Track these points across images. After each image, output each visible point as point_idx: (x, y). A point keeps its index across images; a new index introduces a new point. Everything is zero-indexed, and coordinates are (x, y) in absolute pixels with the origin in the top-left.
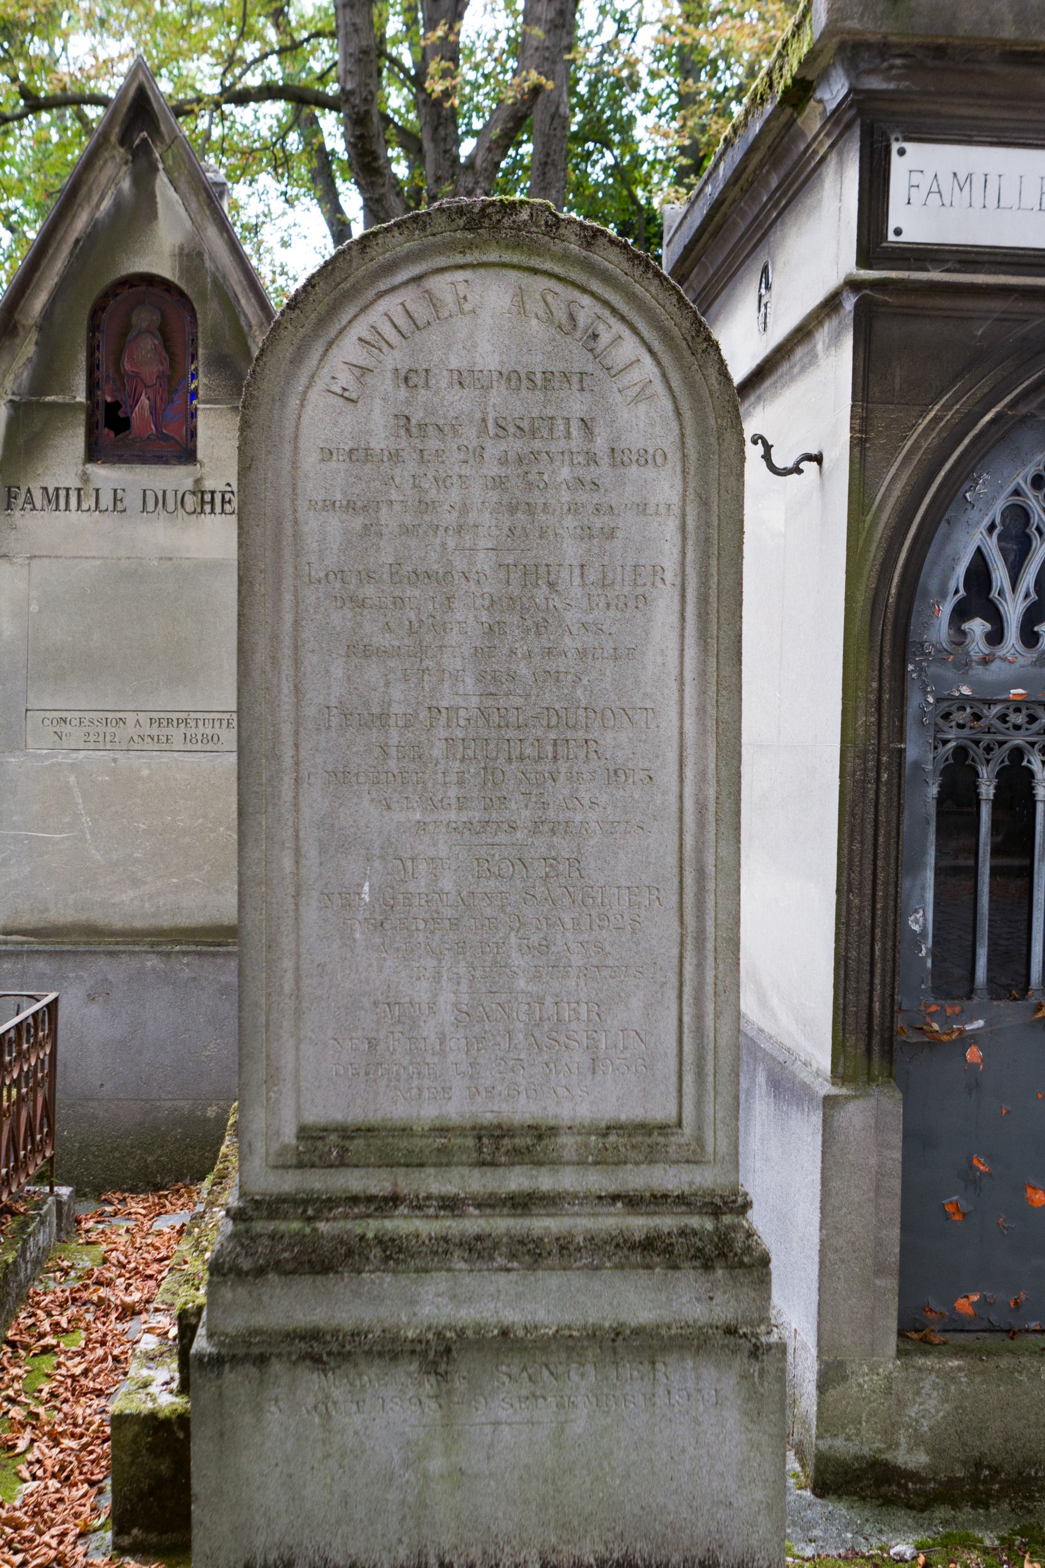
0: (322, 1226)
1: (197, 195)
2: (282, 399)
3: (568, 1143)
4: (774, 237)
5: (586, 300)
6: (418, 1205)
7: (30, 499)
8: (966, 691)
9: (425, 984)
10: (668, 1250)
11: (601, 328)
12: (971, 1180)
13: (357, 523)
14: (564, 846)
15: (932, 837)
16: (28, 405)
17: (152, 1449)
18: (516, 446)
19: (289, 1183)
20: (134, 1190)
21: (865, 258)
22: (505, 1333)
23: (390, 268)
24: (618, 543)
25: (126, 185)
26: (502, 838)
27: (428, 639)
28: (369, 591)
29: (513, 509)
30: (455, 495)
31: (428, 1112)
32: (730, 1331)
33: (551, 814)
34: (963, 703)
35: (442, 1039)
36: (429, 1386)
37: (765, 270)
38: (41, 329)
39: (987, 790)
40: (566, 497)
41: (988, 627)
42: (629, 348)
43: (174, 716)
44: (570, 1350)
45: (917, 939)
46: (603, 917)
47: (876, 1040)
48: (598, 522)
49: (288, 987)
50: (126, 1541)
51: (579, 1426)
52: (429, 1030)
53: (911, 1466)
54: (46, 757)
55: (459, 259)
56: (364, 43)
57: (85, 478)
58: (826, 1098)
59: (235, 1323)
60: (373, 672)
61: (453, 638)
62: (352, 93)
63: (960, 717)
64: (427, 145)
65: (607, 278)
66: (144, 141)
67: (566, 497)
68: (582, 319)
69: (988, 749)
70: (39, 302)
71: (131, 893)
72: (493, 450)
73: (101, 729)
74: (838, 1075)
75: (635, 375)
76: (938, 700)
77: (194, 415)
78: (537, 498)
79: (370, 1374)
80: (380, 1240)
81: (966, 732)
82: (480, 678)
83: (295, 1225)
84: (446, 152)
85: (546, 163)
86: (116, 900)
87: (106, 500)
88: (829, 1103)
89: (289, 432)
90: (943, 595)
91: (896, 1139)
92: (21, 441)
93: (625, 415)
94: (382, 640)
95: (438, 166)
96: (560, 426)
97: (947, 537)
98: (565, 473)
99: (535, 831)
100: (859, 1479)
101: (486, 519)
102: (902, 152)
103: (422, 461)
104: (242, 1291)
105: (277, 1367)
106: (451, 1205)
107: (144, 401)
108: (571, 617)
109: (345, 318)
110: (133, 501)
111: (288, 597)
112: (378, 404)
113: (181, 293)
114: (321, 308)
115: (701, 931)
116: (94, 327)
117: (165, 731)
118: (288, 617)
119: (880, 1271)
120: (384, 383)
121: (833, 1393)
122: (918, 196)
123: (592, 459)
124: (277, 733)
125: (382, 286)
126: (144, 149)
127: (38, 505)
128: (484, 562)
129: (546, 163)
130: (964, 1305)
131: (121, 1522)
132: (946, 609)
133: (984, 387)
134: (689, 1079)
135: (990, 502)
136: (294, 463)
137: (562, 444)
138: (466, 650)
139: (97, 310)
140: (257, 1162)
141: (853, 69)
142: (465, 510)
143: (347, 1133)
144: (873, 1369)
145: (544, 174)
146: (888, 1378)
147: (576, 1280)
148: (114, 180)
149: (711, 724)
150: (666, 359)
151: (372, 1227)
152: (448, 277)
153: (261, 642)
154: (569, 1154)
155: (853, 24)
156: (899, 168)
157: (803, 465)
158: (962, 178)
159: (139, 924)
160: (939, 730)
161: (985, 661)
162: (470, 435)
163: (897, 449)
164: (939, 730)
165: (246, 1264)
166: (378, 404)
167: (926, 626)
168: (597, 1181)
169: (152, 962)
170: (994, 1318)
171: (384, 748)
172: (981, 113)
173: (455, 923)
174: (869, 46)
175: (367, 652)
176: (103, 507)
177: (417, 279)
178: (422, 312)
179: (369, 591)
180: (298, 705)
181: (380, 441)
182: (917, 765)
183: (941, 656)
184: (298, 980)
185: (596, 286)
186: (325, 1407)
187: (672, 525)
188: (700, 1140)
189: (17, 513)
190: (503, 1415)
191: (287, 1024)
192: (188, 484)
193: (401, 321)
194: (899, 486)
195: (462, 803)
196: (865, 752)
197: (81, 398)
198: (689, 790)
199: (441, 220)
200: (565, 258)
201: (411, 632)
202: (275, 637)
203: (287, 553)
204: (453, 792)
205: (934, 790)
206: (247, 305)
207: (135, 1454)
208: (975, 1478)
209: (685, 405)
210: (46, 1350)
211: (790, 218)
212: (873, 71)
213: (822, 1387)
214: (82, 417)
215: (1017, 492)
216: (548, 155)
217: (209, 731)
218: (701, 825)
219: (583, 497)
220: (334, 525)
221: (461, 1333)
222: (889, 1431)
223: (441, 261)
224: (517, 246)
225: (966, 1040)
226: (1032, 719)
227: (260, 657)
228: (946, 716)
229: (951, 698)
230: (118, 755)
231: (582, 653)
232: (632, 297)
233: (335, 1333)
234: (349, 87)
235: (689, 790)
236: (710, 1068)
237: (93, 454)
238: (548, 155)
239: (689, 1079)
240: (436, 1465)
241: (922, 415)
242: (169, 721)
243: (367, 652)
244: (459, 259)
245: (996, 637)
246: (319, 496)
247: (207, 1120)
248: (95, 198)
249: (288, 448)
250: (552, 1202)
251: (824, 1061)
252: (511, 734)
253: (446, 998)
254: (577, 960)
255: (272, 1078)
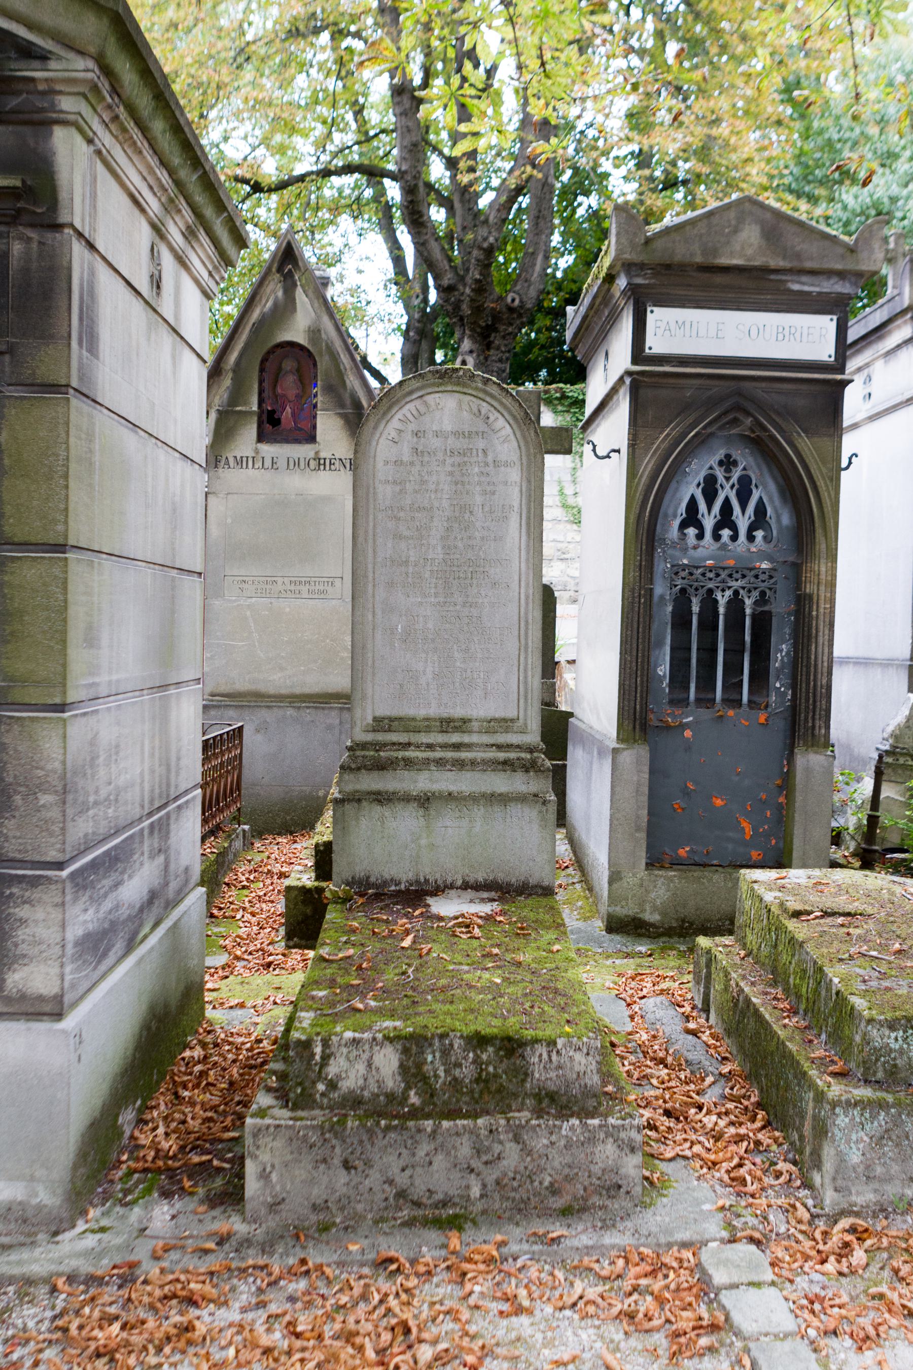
0: (382, 754)
1: (318, 298)
2: (370, 442)
3: (475, 725)
4: (609, 337)
5: (484, 404)
6: (418, 746)
7: (227, 462)
8: (685, 561)
9: (421, 664)
10: (512, 765)
11: (491, 415)
12: (686, 793)
13: (398, 488)
14: (475, 612)
15: (669, 631)
16: (227, 412)
17: (303, 902)
18: (458, 459)
19: (369, 737)
20: (279, 834)
21: (636, 359)
22: (450, 794)
23: (411, 393)
24: (496, 496)
25: (280, 294)
26: (451, 608)
27: (424, 532)
28: (402, 514)
29: (456, 483)
30: (434, 478)
31: (422, 713)
32: (536, 795)
33: (470, 599)
34: (684, 567)
35: (428, 684)
36: (421, 812)
37: (607, 354)
38: (234, 371)
39: (696, 609)
40: (476, 479)
41: (697, 531)
42: (501, 422)
43: (303, 579)
44: (474, 800)
45: (661, 679)
46: (490, 639)
47: (638, 722)
48: (488, 488)
49: (370, 663)
50: (291, 943)
51: (477, 829)
52: (423, 681)
53: (652, 920)
54: (235, 601)
55: (437, 389)
56: (414, 139)
57: (257, 451)
58: (614, 749)
59: (349, 788)
60: (403, 545)
61: (433, 532)
62: (405, 172)
63: (683, 574)
64: (457, 205)
65: (492, 396)
66: (290, 270)
67: (476, 479)
68: (483, 412)
69: (696, 589)
70: (233, 357)
71: (279, 675)
72: (449, 461)
73: (264, 586)
74: (619, 739)
75: (503, 433)
76: (672, 566)
77: (315, 417)
78: (466, 479)
79: (399, 806)
80: (403, 759)
81: (686, 581)
82: (443, 547)
83: (372, 753)
84: (470, 209)
85: (538, 217)
86: (271, 678)
87: (268, 463)
88: (615, 751)
89: (372, 454)
90: (675, 516)
91: (646, 769)
92: (223, 431)
93: (499, 448)
94: (406, 533)
95: (464, 219)
96: (474, 452)
97: (677, 489)
98: (476, 470)
99: (464, 606)
100: (627, 925)
101: (446, 487)
102: (652, 312)
103: (422, 465)
104: (352, 776)
105: (364, 803)
106: (430, 747)
107: (288, 409)
108: (478, 524)
109: (393, 411)
110: (282, 463)
111: (371, 517)
112: (406, 444)
113: (308, 351)
114: (385, 408)
115: (527, 644)
116: (262, 370)
117: (298, 588)
118: (371, 524)
119: (638, 829)
120: (408, 436)
121: (615, 886)
122: (660, 332)
123: (487, 464)
124: (366, 568)
125: (408, 399)
126: (290, 274)
127: (232, 465)
128: (445, 504)
129: (538, 217)
130: (682, 852)
131: (289, 936)
132: (676, 523)
133: (691, 419)
134: (522, 701)
135: (697, 474)
136: (374, 467)
137: (475, 459)
138: (439, 537)
139: (264, 360)
140: (357, 730)
141: (629, 274)
142: (438, 483)
143: (391, 720)
144: (634, 875)
145: (537, 224)
146: (641, 879)
147: (477, 775)
148: (274, 291)
149: (531, 566)
150: (515, 426)
151: (400, 754)
152: (433, 396)
153: (361, 533)
154: (475, 729)
155: (627, 256)
156: (651, 319)
157: (612, 454)
158: (680, 323)
159: (283, 691)
160: (673, 580)
161: (695, 548)
162: (440, 455)
163: (650, 448)
164: (673, 580)
165: (353, 766)
166: (406, 444)
167: (667, 531)
168: (486, 739)
169: (290, 712)
170: (696, 858)
171: (407, 574)
172: (690, 293)
173: (433, 640)
174: (635, 265)
175: (401, 537)
176: (266, 466)
177: (421, 396)
178: (422, 409)
179: (402, 514)
180: (375, 557)
181: (406, 458)
182: (662, 597)
183: (674, 545)
184: (374, 662)
185: (488, 399)
186: (382, 819)
187: (517, 490)
188: (526, 725)
189: (220, 470)
190: (448, 824)
191: (369, 678)
192: (312, 454)
193: (415, 413)
194: (650, 466)
195: (436, 595)
196: (634, 589)
197: (255, 408)
198: (523, 591)
199: (430, 375)
200: (476, 389)
201: (417, 530)
202: (366, 532)
203: (371, 500)
204: (433, 591)
205: (670, 609)
206: (344, 359)
207: (296, 904)
208: (682, 927)
209: (522, 444)
210: (244, 887)
211: (613, 331)
212: (637, 276)
213: (610, 883)
214: (255, 418)
215: (711, 468)
216: (540, 211)
217: (322, 588)
218: (527, 604)
219: (483, 479)
220: (389, 489)
221: (433, 794)
222: (642, 904)
223: (430, 390)
224: (458, 384)
225: (683, 727)
226: (718, 575)
227: (361, 539)
228: (676, 573)
229: (678, 565)
230: (273, 600)
231: (482, 538)
232: (501, 403)
233: (386, 792)
234: (404, 168)
235: (523, 591)
236: (529, 696)
237: (261, 438)
238: (540, 211)
239: (522, 701)
240: (423, 842)
241: (661, 433)
242: (300, 582)
243: (401, 537)
244: (437, 389)
245: (700, 536)
246: (383, 478)
247: (318, 797)
248: (264, 301)
249: (371, 460)
250: (469, 746)
251: (613, 732)
252: (455, 569)
253: (429, 670)
254: (479, 655)
255: (364, 697)
